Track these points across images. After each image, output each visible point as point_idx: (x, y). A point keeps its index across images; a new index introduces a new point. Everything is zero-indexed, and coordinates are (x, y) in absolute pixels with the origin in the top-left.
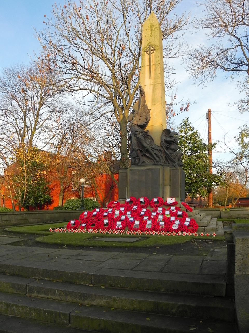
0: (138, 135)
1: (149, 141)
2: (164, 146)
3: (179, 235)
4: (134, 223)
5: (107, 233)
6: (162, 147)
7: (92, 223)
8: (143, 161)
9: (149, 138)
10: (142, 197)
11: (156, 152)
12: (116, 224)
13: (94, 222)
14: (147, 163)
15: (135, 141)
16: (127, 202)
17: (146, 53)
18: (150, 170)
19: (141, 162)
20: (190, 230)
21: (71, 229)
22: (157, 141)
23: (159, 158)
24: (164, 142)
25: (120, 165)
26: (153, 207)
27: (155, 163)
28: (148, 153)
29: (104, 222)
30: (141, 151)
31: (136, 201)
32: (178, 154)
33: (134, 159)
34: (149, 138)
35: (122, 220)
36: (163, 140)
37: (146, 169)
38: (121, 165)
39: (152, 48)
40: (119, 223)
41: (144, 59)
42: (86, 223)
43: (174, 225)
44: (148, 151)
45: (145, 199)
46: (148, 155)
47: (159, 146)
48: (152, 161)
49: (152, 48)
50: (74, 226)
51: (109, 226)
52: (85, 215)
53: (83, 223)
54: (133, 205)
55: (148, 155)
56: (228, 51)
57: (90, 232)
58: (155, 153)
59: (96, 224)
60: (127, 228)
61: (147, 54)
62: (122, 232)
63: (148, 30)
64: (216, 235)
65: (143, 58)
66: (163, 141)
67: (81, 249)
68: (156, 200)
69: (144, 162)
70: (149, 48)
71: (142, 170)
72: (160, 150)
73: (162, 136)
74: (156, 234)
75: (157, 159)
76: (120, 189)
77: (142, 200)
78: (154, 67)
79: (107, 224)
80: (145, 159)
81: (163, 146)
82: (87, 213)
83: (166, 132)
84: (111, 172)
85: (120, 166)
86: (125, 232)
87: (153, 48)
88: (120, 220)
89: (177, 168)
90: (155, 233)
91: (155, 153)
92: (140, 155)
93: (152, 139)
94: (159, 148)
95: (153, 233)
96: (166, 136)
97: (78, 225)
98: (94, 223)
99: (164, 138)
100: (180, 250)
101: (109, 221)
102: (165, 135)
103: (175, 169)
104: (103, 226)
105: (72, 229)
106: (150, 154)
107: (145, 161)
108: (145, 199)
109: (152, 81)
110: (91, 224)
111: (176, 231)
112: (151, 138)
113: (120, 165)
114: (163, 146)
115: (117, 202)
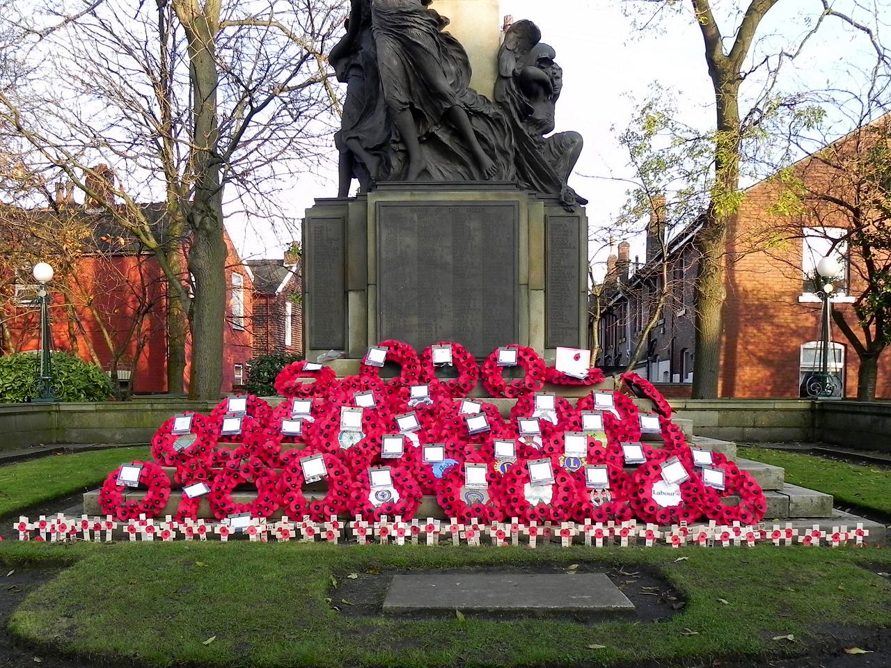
0: (414, 31)
1: (453, 68)
2: (512, 100)
3: (287, 540)
4: (462, 479)
5: (485, 539)
6: (501, 104)
7: (237, 477)
8: (423, 166)
9: (454, 54)
10: (441, 343)
11: (480, 125)
12: (366, 484)
13: (247, 470)
14: (437, 177)
15: (395, 63)
16: (373, 367)
18: (475, 207)
19: (415, 169)
20: (742, 511)
21: (423, 520)
22: (482, 82)
23: (493, 158)
24: (515, 83)
25: (194, 211)
26: (506, 394)
27: (472, 178)
28: (450, 128)
29: (302, 473)
30: (418, 116)
31: (418, 361)
32: (568, 146)
33: (376, 155)
34: (454, 54)
35: (392, 462)
36: (510, 74)
37: (458, 205)
38: (198, 209)
40: (381, 479)
42: (209, 479)
43: (657, 487)
44: (449, 119)
45: (458, 352)
46: (444, 137)
47: (488, 101)
48: (460, 169)
50: (142, 495)
51: (335, 494)
52: (181, 434)
53: (191, 481)
54: (407, 381)
55: (444, 137)
57: (408, 538)
58: (476, 132)
59: (258, 484)
60: (426, 504)
62: (400, 530)
64: (866, 533)
66: (506, 78)
68: (507, 357)
69: (425, 172)
71: (438, 206)
72: (495, 122)
73: (506, 51)
74: (661, 541)
75: (487, 161)
76: (310, 300)
77: (442, 355)
79: (321, 485)
80: (425, 157)
81: (509, 101)
82: (193, 422)
83: (519, 38)
84: (158, 240)
85: (192, 214)
86: (36, 525)
88: (380, 462)
89: (573, 208)
90: (632, 533)
91: (476, 132)
92: (413, 134)
93: (466, 64)
94: (491, 111)
95: (565, 532)
97: (163, 490)
98: (249, 478)
99: (511, 66)
101: (329, 465)
102: (513, 51)
103: (563, 213)
104: (300, 492)
105: (306, 517)
106: (459, 134)
107: (429, 168)
108: (456, 351)
110: (234, 484)
111: (543, 514)
112: (459, 56)
113: (194, 211)
115: (318, 367)
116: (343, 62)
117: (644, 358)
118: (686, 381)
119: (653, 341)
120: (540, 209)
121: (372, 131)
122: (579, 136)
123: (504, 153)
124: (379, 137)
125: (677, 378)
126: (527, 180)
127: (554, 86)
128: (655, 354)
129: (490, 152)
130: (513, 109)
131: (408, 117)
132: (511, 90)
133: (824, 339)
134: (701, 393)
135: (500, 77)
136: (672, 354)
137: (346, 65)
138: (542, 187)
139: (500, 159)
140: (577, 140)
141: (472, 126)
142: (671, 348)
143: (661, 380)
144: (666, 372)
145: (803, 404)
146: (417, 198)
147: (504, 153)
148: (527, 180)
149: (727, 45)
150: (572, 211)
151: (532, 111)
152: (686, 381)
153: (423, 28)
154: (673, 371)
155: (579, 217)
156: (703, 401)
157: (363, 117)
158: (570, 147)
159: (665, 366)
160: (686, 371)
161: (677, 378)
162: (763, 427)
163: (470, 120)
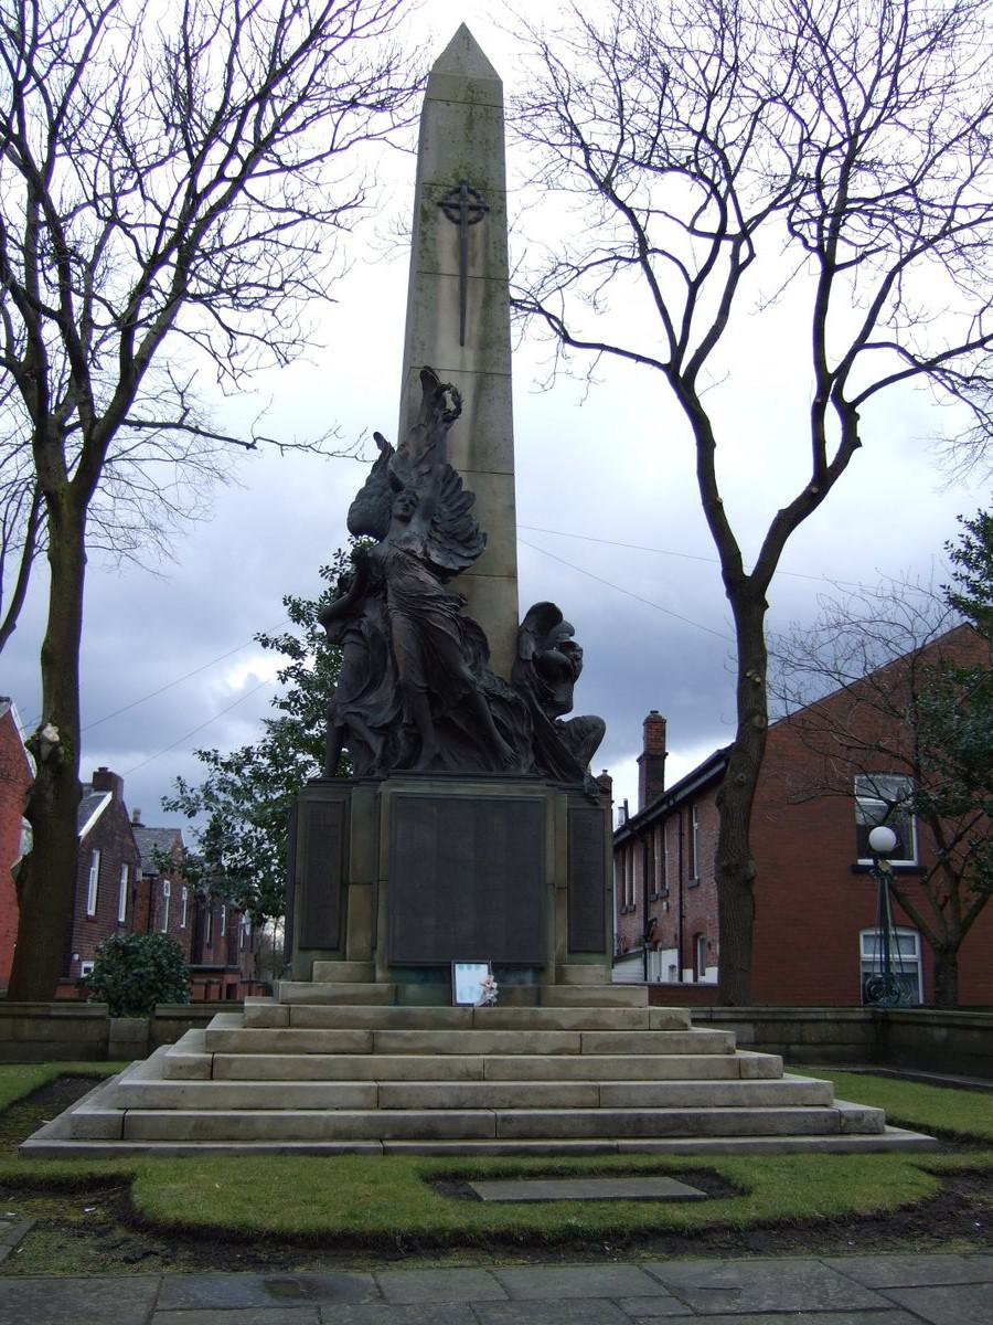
1: (470, 650)
2: (531, 683)
6: (519, 688)
17: (442, 215)
22: (500, 663)
30: (434, 701)
32: (589, 732)
37: (477, 803)
39: (473, 200)
41: (434, 240)
49: (473, 200)
55: (460, 723)
56: (791, 162)
58: (494, 718)
61: (450, 218)
63: (452, 105)
65: (429, 234)
67: (979, 1091)
70: (458, 191)
78: (481, 291)
81: (527, 683)
87: (478, 197)
91: (494, 718)
94: (511, 695)
96: (435, 535)
100: (169, 1260)
103: (587, 806)
106: (477, 719)
109: (470, 356)
114: (527, 683)
116: (339, 624)
117: (638, 944)
118: (702, 979)
119: (651, 922)
120: (564, 801)
121: (377, 708)
122: (603, 723)
123: (522, 739)
124: (386, 716)
125: (688, 976)
126: (548, 768)
127: (575, 667)
128: (655, 939)
129: (508, 737)
130: (532, 693)
131: (425, 701)
132: (531, 672)
133: (884, 925)
134: (543, 1002)
135: (519, 660)
136: (681, 941)
137: (342, 628)
138: (562, 775)
139: (519, 746)
140: (600, 726)
141: (492, 712)
142: (678, 932)
143: (665, 979)
144: (672, 967)
145: (859, 1013)
146: (436, 791)
147: (522, 739)
148: (546, 767)
149: (749, 567)
150: (596, 804)
151: (552, 696)
152: (702, 979)
153: (447, 615)
154: (682, 965)
155: (603, 810)
156: (733, 1009)
157: (367, 691)
158: (590, 734)
159: (670, 957)
160: (702, 963)
161: (688, 976)
162: (811, 1044)
163: (489, 704)
